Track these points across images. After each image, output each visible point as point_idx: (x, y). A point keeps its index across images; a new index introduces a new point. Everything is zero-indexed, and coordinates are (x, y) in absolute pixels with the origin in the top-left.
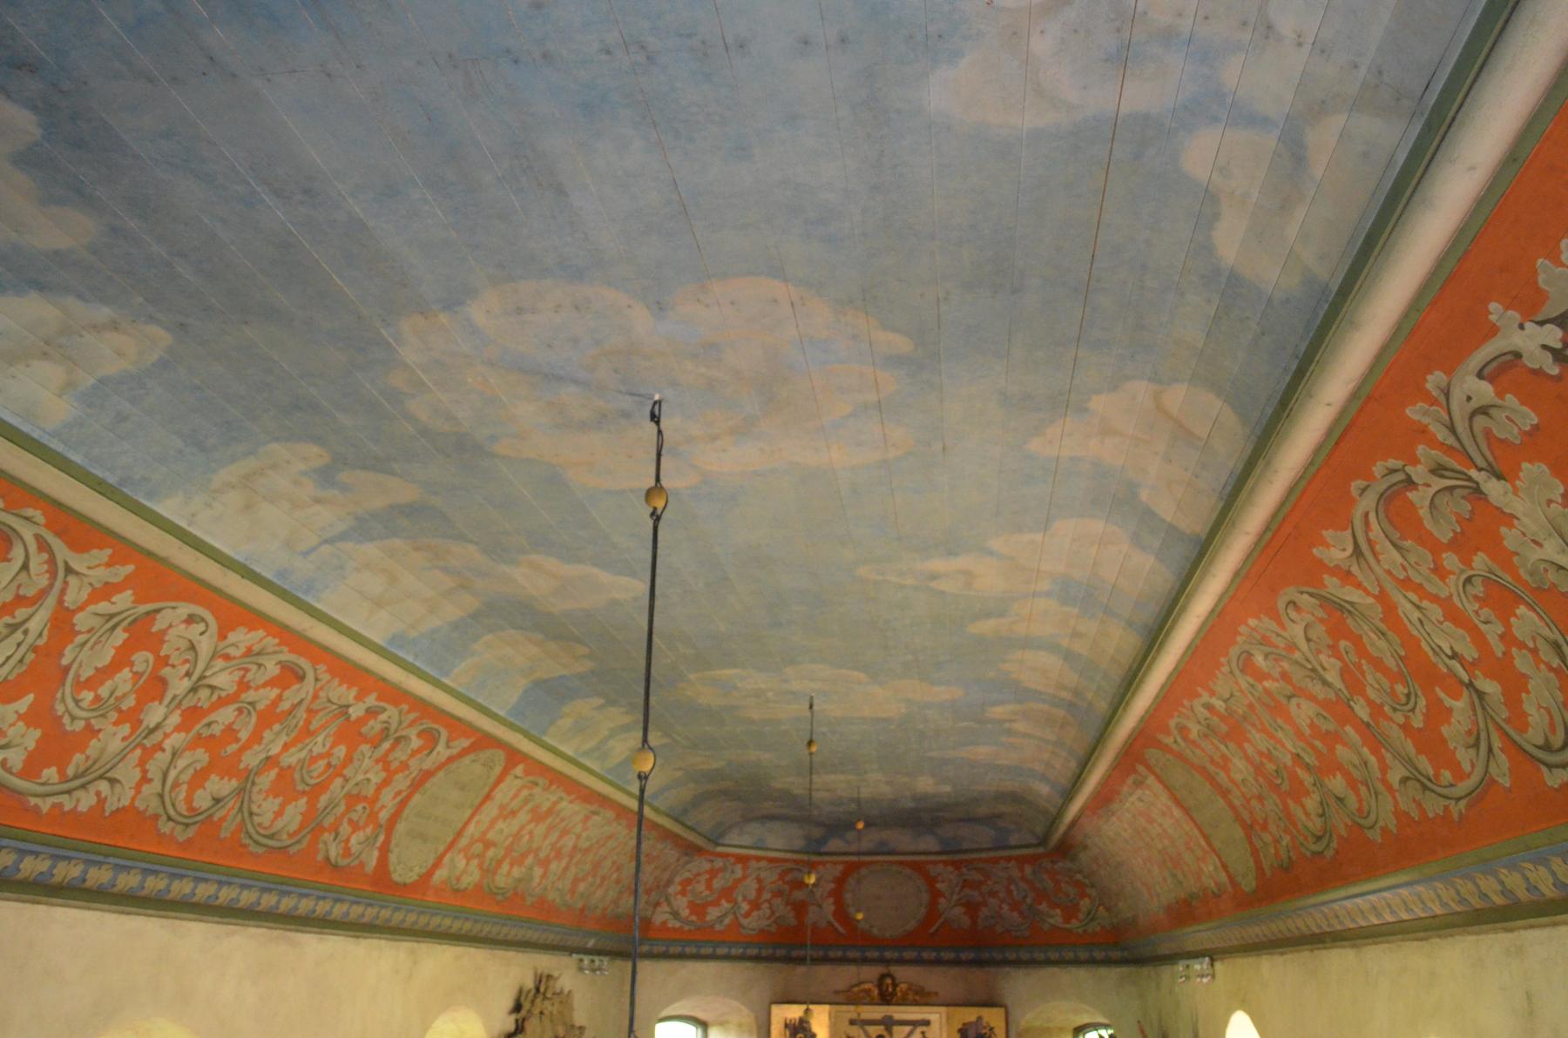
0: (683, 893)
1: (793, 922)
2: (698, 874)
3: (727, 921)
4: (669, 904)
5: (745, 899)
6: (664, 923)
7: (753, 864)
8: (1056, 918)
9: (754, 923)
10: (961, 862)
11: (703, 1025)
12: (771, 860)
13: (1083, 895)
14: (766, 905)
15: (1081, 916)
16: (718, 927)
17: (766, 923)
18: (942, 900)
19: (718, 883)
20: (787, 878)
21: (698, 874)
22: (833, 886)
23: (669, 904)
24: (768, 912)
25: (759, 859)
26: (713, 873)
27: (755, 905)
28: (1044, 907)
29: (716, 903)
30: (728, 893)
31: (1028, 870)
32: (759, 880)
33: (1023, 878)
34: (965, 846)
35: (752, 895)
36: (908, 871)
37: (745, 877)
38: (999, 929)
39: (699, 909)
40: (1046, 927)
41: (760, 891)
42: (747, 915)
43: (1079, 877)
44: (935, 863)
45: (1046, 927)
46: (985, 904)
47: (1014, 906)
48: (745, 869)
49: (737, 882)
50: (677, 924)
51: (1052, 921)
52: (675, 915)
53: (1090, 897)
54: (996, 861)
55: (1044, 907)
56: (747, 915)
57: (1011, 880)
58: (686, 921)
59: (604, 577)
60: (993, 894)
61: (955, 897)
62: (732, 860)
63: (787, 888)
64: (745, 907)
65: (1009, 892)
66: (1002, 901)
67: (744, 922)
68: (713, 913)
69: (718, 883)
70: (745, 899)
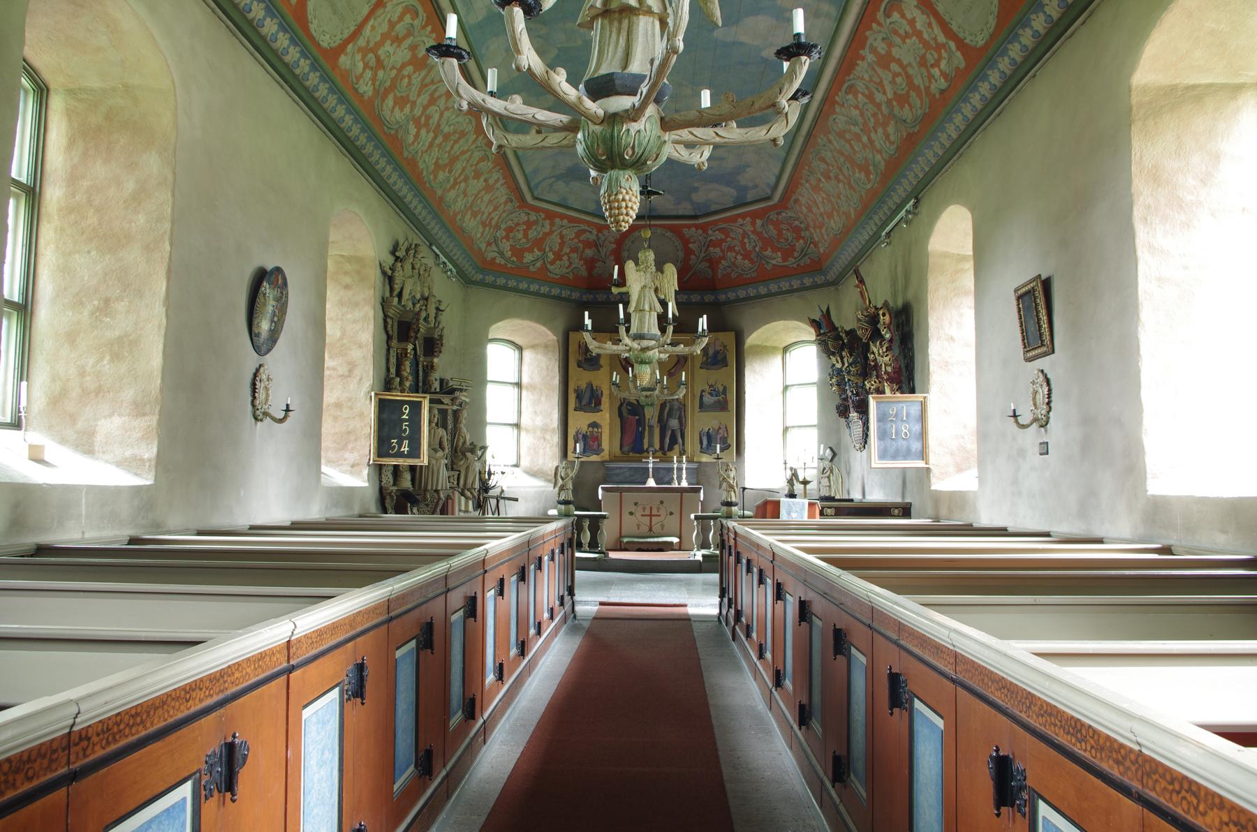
0: (507, 238)
1: (585, 274)
2: (518, 224)
3: (538, 264)
4: (497, 246)
5: (551, 250)
6: (494, 259)
7: (557, 220)
8: (777, 259)
9: (557, 269)
10: (708, 224)
11: (520, 349)
12: (571, 220)
13: (799, 238)
14: (565, 258)
15: (796, 254)
16: (532, 269)
17: (565, 271)
18: (693, 257)
19: (532, 234)
20: (582, 238)
21: (518, 224)
22: (614, 246)
23: (497, 246)
24: (567, 264)
25: (562, 217)
26: (529, 225)
27: (558, 256)
28: (768, 253)
29: (530, 250)
30: (539, 243)
31: (759, 222)
32: (562, 237)
33: (754, 232)
34: (714, 208)
35: (556, 248)
36: (669, 234)
37: (551, 232)
38: (733, 275)
39: (518, 252)
40: (769, 267)
41: (562, 244)
42: (552, 263)
43: (797, 223)
44: (689, 227)
45: (769, 267)
46: (723, 258)
47: (746, 256)
48: (552, 224)
49: (547, 235)
50: (503, 262)
51: (774, 262)
52: (501, 254)
53: (803, 238)
54: (733, 219)
55: (768, 253)
56: (552, 263)
57: (745, 234)
58: (507, 260)
59: (444, 773)
60: (731, 249)
61: (702, 255)
62: (543, 215)
63: (581, 245)
64: (551, 256)
65: (743, 244)
66: (737, 253)
67: (551, 268)
68: (528, 257)
69: (532, 234)
70: (551, 250)
